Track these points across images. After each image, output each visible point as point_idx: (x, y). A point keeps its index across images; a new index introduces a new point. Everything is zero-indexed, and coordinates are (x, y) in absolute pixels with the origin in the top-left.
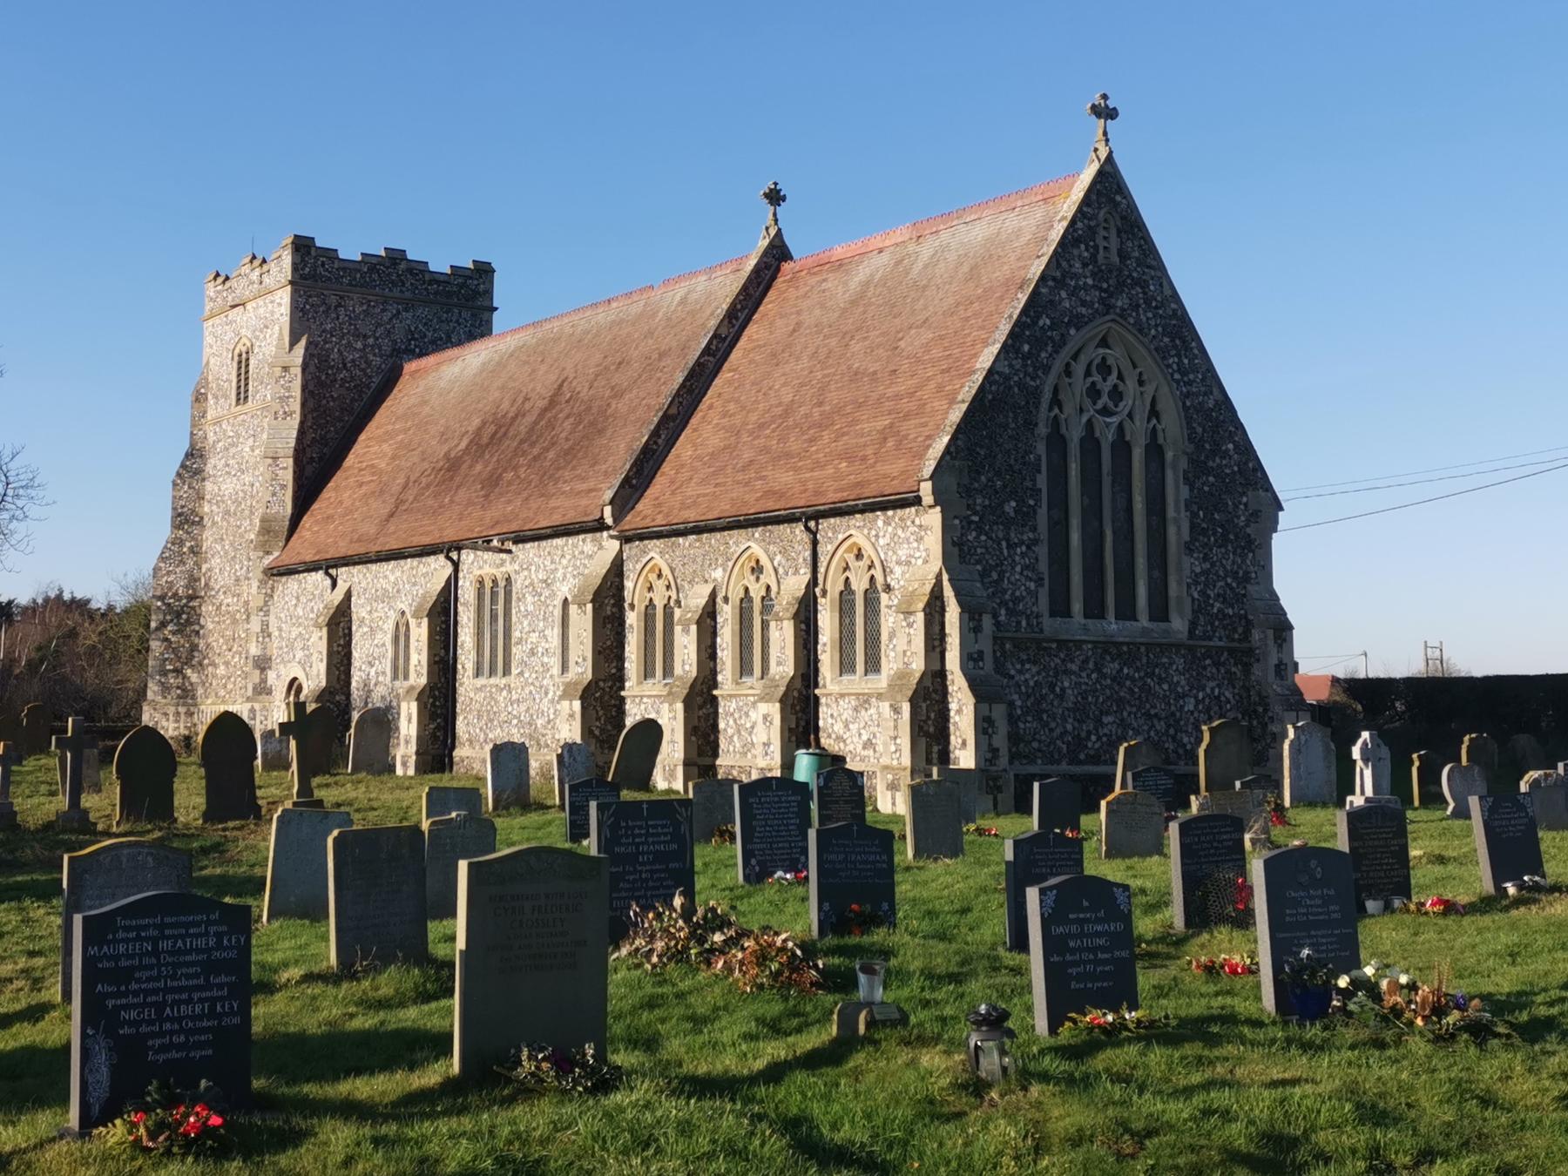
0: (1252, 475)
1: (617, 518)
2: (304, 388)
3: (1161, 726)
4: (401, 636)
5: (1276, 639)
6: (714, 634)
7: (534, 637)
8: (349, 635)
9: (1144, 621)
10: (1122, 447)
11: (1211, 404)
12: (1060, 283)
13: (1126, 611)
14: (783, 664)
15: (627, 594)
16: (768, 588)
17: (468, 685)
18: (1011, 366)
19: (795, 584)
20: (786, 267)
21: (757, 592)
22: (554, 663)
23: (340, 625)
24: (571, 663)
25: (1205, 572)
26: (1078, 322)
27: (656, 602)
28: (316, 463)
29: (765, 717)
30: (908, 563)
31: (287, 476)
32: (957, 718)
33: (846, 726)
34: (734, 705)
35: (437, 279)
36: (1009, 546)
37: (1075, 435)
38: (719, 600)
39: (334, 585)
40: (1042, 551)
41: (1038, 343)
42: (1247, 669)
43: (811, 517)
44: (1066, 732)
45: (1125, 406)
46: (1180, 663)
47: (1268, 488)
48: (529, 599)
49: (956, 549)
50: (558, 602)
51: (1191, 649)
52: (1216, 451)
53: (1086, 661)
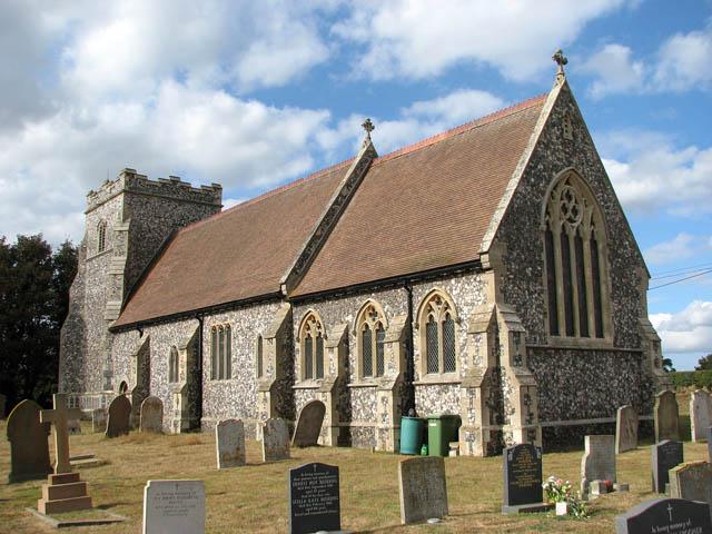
0: (637, 259)
1: (288, 291)
2: (130, 241)
3: (603, 396)
4: (174, 358)
6: (348, 352)
7: (243, 358)
8: (148, 359)
9: (593, 338)
10: (579, 240)
11: (617, 220)
12: (547, 147)
13: (585, 333)
14: (393, 372)
15: (295, 332)
16: (381, 324)
17: (210, 385)
18: (526, 190)
19: (396, 324)
20: (376, 162)
21: (372, 326)
22: (254, 371)
23: (144, 355)
24: (264, 371)
26: (556, 168)
27: (312, 336)
28: (133, 282)
29: (383, 399)
30: (473, 304)
31: (121, 283)
32: (508, 396)
33: (433, 402)
34: (360, 392)
35: (194, 192)
36: (530, 294)
37: (557, 232)
38: (350, 333)
39: (141, 335)
40: (545, 297)
41: (539, 178)
42: (639, 362)
43: (407, 281)
45: (579, 218)
47: (644, 266)
48: (240, 338)
49: (503, 295)
50: (256, 338)
52: (621, 245)
53: (568, 360)
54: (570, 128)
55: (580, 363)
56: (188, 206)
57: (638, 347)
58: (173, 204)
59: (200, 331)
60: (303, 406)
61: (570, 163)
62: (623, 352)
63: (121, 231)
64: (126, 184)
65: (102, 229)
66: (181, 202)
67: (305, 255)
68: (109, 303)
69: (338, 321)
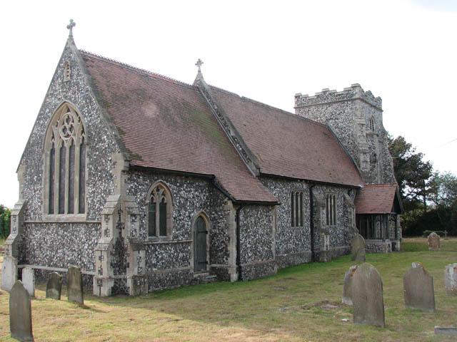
3: (76, 254)
5: (105, 218)
25: (94, 192)
35: (312, 99)
37: (57, 147)
44: (47, 255)
46: (83, 230)
51: (87, 224)
55: (61, 232)
56: (335, 105)
58: (325, 107)
62: (94, 223)
66: (330, 104)
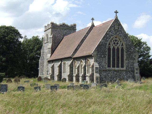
2: (53, 40)
12: (110, 32)
23: (53, 67)
26: (112, 36)
28: (53, 50)
31: (50, 50)
37: (112, 48)
41: (107, 38)
54: (117, 27)
57: (134, 70)
59: (61, 63)
60: (63, 78)
61: (116, 34)
63: (50, 38)
64: (51, 26)
65: (47, 35)
66: (65, 29)
67: (76, 49)
68: (48, 55)
69: (77, 64)
